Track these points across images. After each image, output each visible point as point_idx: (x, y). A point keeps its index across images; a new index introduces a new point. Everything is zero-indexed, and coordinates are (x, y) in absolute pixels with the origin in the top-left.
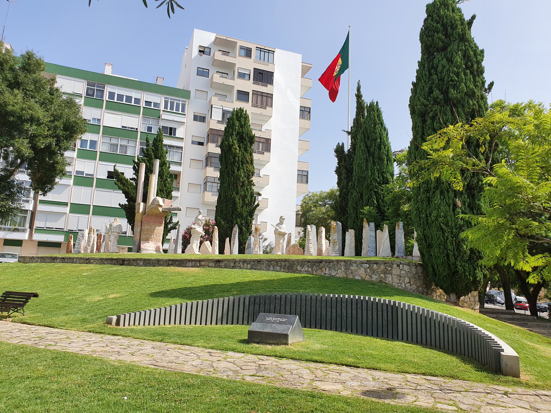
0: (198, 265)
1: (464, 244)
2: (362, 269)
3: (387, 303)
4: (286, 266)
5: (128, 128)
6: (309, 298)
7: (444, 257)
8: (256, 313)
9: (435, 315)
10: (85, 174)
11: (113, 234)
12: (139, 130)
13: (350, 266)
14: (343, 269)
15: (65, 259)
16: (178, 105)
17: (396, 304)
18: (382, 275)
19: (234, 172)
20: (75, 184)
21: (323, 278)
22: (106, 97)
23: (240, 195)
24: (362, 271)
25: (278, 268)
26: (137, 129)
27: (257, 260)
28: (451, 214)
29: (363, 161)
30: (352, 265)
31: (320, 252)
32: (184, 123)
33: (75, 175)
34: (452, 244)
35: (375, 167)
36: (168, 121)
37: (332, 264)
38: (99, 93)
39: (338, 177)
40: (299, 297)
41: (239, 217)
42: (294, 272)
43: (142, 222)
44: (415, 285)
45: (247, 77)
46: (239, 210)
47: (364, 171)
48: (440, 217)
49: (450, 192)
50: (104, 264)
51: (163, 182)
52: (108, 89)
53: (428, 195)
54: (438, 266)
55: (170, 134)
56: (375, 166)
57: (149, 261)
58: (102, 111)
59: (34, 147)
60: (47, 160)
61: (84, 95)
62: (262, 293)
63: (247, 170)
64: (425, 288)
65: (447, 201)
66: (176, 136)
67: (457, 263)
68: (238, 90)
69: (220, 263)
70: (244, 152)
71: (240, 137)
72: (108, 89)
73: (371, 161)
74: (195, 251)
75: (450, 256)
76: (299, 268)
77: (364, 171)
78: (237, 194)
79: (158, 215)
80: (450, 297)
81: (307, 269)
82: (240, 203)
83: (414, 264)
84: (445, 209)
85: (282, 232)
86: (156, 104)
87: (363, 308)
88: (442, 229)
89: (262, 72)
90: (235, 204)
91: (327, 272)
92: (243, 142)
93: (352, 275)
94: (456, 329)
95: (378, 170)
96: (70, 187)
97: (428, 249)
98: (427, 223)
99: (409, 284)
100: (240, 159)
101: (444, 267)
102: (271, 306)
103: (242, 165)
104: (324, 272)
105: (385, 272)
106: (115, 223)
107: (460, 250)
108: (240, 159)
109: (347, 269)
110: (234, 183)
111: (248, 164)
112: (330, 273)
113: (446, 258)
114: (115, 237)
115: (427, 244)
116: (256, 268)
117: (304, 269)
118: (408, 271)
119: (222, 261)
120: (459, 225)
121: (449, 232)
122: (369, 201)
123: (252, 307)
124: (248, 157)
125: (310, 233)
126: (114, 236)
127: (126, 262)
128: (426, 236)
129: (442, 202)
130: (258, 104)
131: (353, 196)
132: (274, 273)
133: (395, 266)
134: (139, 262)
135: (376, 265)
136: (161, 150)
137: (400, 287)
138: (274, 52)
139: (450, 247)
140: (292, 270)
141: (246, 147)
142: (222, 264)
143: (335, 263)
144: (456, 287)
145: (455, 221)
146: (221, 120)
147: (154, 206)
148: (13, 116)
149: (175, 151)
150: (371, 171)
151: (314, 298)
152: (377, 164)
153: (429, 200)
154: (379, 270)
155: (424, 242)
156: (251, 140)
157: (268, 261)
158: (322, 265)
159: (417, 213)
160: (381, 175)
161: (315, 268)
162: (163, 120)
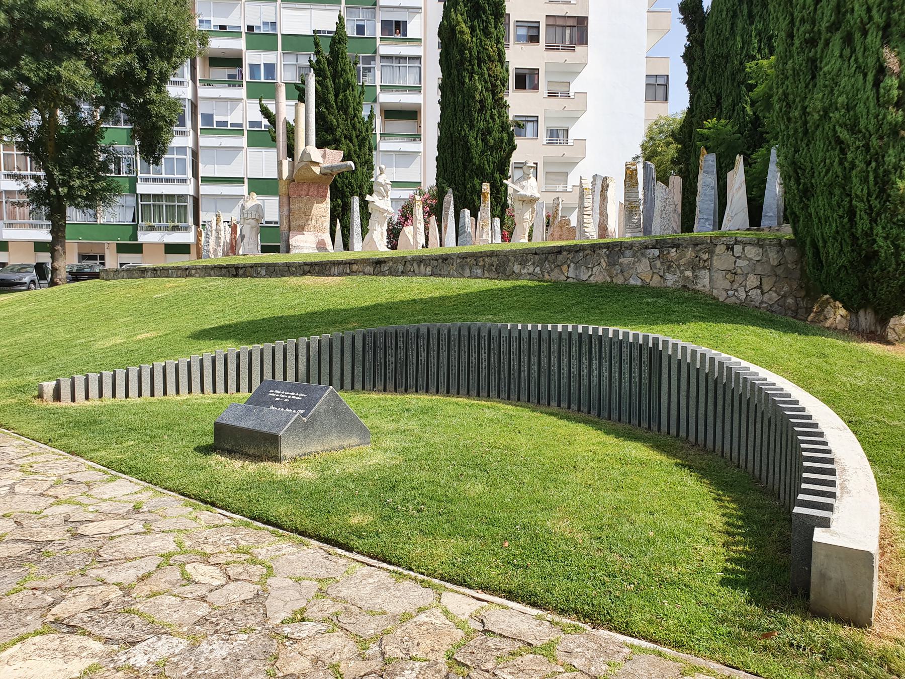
0: (348, 271)
2: (645, 261)
3: (641, 342)
4: (493, 265)
5: (324, 32)
6: (484, 333)
7: (841, 217)
8: (379, 367)
9: (733, 376)
10: (229, 125)
11: (248, 221)
13: (619, 257)
14: (604, 264)
15: (157, 270)
17: (658, 344)
18: (688, 273)
19: (463, 83)
20: (251, 144)
21: (558, 287)
24: (643, 267)
25: (479, 271)
27: (441, 257)
28: (868, 98)
29: (724, 16)
30: (622, 254)
31: (603, 229)
32: (421, 8)
33: (248, 129)
34: (866, 180)
35: (753, 27)
36: (392, 9)
37: (581, 254)
39: (690, 73)
40: (464, 332)
41: (477, 175)
42: (508, 278)
43: (289, 198)
44: (775, 291)
46: (476, 161)
47: (727, 39)
48: (837, 109)
49: (870, 32)
50: (210, 275)
51: (349, 120)
53: (811, 55)
54: (825, 242)
56: (752, 23)
58: (276, 6)
59: (99, 75)
60: (133, 97)
63: (490, 75)
64: (803, 299)
65: (861, 60)
66: (408, 37)
67: (875, 232)
69: (382, 265)
70: (483, 38)
71: (473, 7)
73: (745, 12)
74: (378, 246)
75: (858, 212)
76: (517, 268)
77: (727, 39)
78: (470, 129)
80: (857, 318)
81: (531, 269)
82: (477, 146)
83: (775, 242)
84: (853, 86)
85: (526, 196)
87: (593, 354)
88: (839, 142)
90: (467, 148)
91: (571, 274)
92: (479, 17)
93: (623, 275)
94: (770, 419)
95: (759, 34)
96: (244, 150)
97: (804, 199)
98: (806, 132)
99: (759, 291)
100: (473, 53)
101: (841, 245)
102: (409, 353)
103: (479, 66)
104: (566, 274)
105: (694, 266)
106: (250, 201)
107: (889, 196)
109: (612, 264)
110: (464, 106)
111: (493, 62)
113: (846, 220)
114: (252, 227)
115: (801, 187)
116: (439, 272)
117: (526, 271)
119: (385, 262)
120: (890, 124)
121: (858, 148)
122: (734, 110)
123: (370, 356)
124: (492, 50)
127: (241, 272)
128: (800, 168)
129: (846, 66)
131: (701, 104)
133: (720, 249)
134: (259, 269)
135: (674, 250)
136: (342, 58)
137: (734, 298)
139: (858, 188)
140: (504, 272)
141: (486, 27)
142: (385, 268)
143: (586, 252)
144: (875, 295)
147: (304, 163)
148: (49, 19)
149: (408, 65)
150: (742, 38)
151: (494, 333)
152: (757, 19)
153: (814, 66)
154: (682, 262)
155: (792, 183)
156: (497, 9)
157: (460, 258)
158: (560, 258)
159: (781, 111)
160: (765, 44)
162: (382, 9)
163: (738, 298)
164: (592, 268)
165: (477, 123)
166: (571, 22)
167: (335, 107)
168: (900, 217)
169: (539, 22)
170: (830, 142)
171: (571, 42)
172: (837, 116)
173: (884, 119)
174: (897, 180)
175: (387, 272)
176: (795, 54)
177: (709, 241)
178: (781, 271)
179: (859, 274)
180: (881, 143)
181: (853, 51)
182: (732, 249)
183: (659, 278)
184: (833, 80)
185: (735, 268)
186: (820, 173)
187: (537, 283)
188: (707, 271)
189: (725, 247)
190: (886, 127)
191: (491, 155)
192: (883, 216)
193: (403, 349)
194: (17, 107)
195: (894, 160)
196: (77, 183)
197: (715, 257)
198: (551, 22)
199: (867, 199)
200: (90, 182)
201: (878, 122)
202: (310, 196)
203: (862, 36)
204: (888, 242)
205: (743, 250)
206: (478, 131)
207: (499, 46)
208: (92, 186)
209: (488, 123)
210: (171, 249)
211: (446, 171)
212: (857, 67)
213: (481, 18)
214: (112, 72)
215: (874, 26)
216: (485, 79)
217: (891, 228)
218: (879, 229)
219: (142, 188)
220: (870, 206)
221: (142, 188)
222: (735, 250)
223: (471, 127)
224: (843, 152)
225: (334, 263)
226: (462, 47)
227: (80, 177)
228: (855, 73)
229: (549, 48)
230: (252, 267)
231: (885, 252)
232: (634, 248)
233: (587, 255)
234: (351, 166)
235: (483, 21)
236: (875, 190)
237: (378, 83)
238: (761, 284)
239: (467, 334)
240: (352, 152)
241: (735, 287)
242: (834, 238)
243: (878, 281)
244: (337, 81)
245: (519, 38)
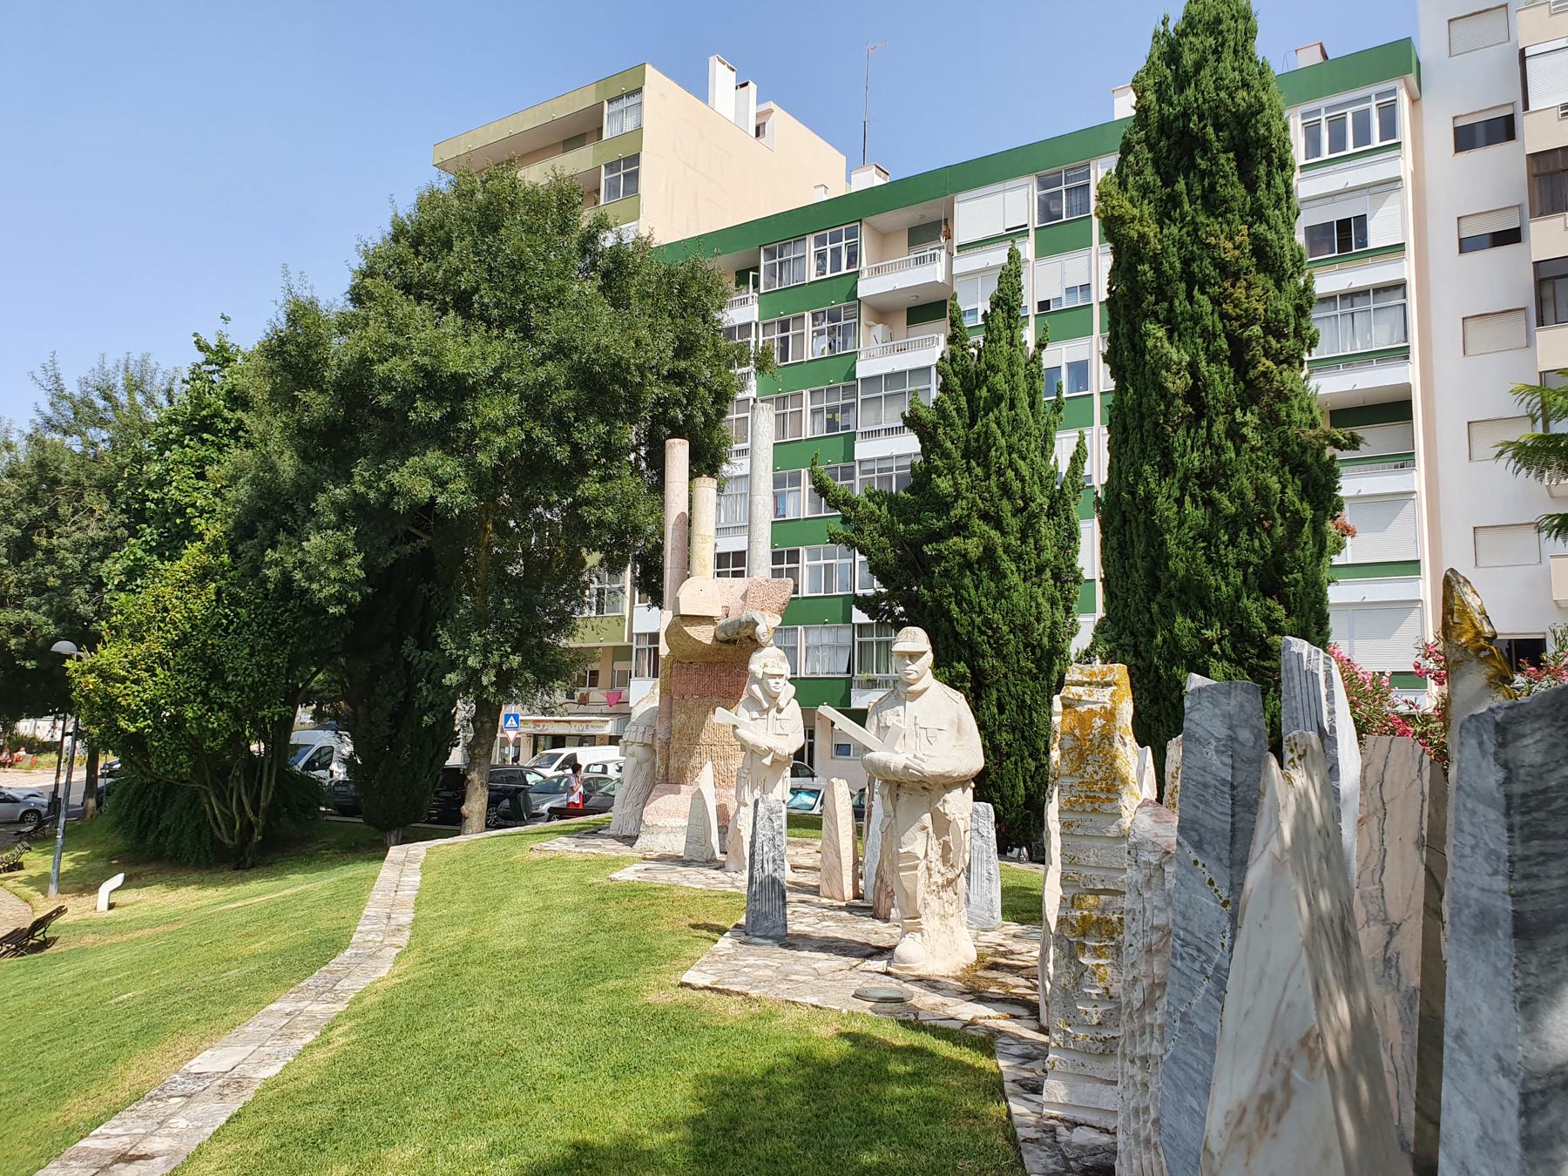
16: (1337, 126)
23: (1179, 475)
51: (994, 478)
55: (1345, 245)
61: (1034, 222)
63: (1224, 316)
70: (1202, 219)
79: (710, 659)
100: (1166, 266)
165: (1182, 456)
191: (1233, 542)
202: (702, 696)
206: (1186, 478)
209: (1218, 450)
213: (1194, 166)
216: (1205, 329)
223: (1167, 469)
235: (1203, 174)
240: (1000, 551)
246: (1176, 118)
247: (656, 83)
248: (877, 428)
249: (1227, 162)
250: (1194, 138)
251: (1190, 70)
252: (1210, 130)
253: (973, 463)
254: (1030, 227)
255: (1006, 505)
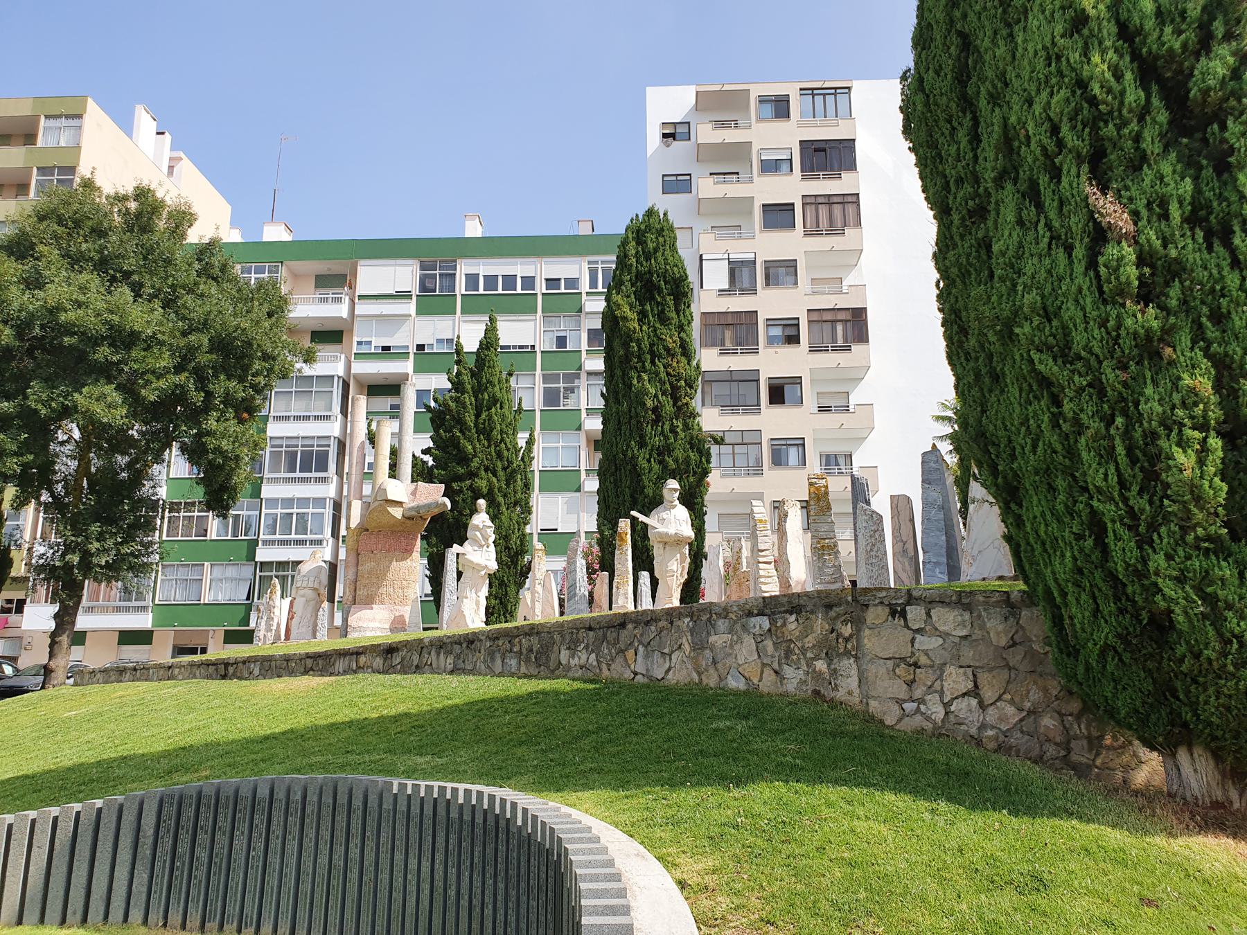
1: (1183, 444)
2: (749, 642)
4: (531, 650)
5: (514, 347)
7: (1079, 537)
11: (301, 592)
12: (537, 349)
13: (708, 634)
14: (687, 647)
19: (630, 386)
22: (461, 287)
24: (746, 651)
26: (533, 347)
28: (1080, 290)
30: (713, 626)
34: (1108, 454)
37: (653, 628)
38: (446, 282)
44: (1012, 702)
45: (785, 167)
49: (1065, 167)
51: (493, 446)
52: (464, 268)
57: (271, 661)
58: (454, 320)
61: (416, 291)
62: (187, 782)
64: (1078, 717)
67: (1152, 566)
68: (764, 205)
70: (658, 325)
71: (644, 286)
72: (464, 268)
75: (1109, 525)
76: (564, 655)
78: (641, 448)
83: (996, 597)
84: (1049, 272)
86: (572, 282)
88: (1045, 382)
89: (822, 145)
91: (640, 668)
92: (652, 298)
93: (717, 670)
97: (1013, 506)
99: (974, 702)
100: (643, 346)
101: (1095, 599)
103: (653, 362)
104: (632, 666)
108: (646, 345)
109: (700, 647)
110: (631, 417)
112: (647, 670)
113: (1089, 543)
115: (1000, 480)
118: (964, 633)
120: (1135, 335)
121: (1081, 390)
125: (760, 525)
126: (304, 599)
127: (231, 670)
130: (821, 225)
132: (454, 681)
133: (876, 614)
135: (793, 618)
136: (489, 367)
137: (918, 718)
138: (849, 88)
139: (1096, 476)
141: (663, 311)
145: (1103, 324)
146: (726, 286)
147: (377, 503)
148: (73, 334)
156: (678, 287)
158: (625, 635)
161: (606, 651)
163: (928, 719)
164: (670, 655)
165: (650, 439)
166: (841, 316)
167: (474, 431)
168: (1200, 531)
169: (798, 319)
170: (1030, 386)
171: (846, 340)
172: (1027, 329)
173: (1119, 327)
174: (1175, 448)
175: (399, 666)
176: (957, 238)
177: (850, 598)
178: (1019, 657)
179: (1150, 664)
180: (1123, 376)
181: (1039, 206)
182: (903, 615)
183: (773, 676)
184: (1012, 266)
185: (913, 654)
186: (1023, 448)
187: (578, 685)
188: (852, 660)
189: (887, 610)
190: (1127, 343)
192: (1163, 530)
193: (206, 833)
194: (14, 448)
195: (1159, 409)
196: (94, 546)
197: (867, 632)
198: (815, 317)
199: (1121, 495)
200: (116, 544)
201: (1108, 333)
203: (1051, 179)
204: (1187, 588)
205: (928, 615)
206: (652, 450)
207: (683, 335)
208: (118, 550)
209: (667, 438)
210: (129, 637)
211: (608, 507)
212: (1052, 238)
213: (655, 299)
214: (152, 398)
215: (1070, 156)
216: (660, 379)
217: (1188, 558)
218: (1158, 561)
219: (262, 554)
220: (1131, 512)
221: (262, 554)
222: (909, 616)
223: (642, 444)
224: (1056, 401)
225: (340, 654)
226: (628, 338)
227: (101, 538)
228: (1050, 248)
229: (814, 349)
230: (244, 662)
231: (1186, 613)
232: (731, 615)
233: (662, 629)
234: (445, 505)
235: (658, 304)
236: (1135, 476)
237: (583, 406)
238: (976, 686)
239: (331, 801)
240: (496, 490)
241: (918, 693)
242: (1077, 584)
243: (1195, 681)
244: (480, 396)
245: (771, 341)
246: (645, 273)
247: (94, 114)
248: (287, 414)
249: (670, 300)
250: (653, 285)
251: (652, 251)
252: (662, 283)
253: (482, 437)
254: (413, 293)
255: (499, 464)
